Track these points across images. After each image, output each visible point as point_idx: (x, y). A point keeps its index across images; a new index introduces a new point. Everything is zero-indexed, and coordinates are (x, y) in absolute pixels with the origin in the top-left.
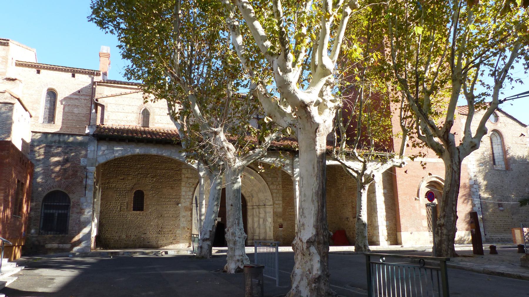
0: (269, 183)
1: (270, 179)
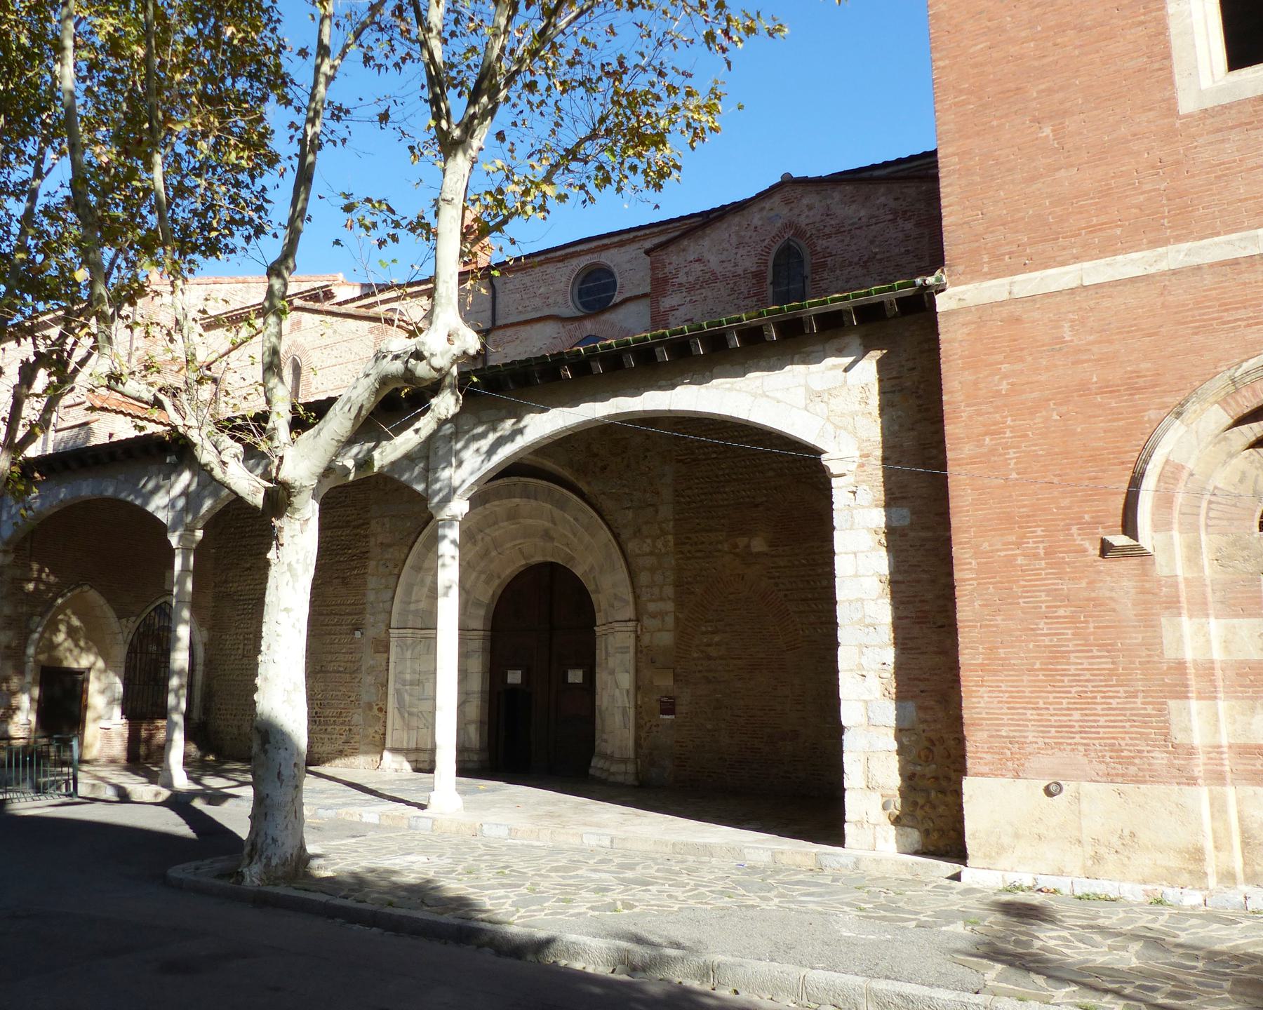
0: (625, 534)
1: (630, 514)
